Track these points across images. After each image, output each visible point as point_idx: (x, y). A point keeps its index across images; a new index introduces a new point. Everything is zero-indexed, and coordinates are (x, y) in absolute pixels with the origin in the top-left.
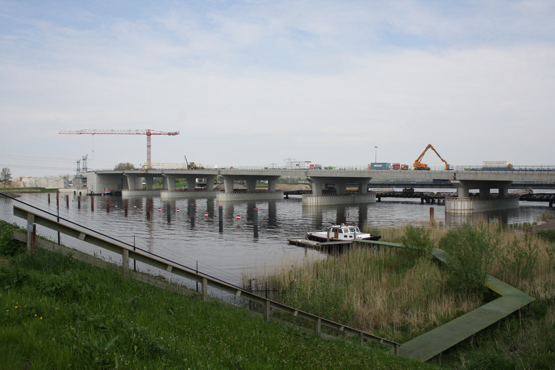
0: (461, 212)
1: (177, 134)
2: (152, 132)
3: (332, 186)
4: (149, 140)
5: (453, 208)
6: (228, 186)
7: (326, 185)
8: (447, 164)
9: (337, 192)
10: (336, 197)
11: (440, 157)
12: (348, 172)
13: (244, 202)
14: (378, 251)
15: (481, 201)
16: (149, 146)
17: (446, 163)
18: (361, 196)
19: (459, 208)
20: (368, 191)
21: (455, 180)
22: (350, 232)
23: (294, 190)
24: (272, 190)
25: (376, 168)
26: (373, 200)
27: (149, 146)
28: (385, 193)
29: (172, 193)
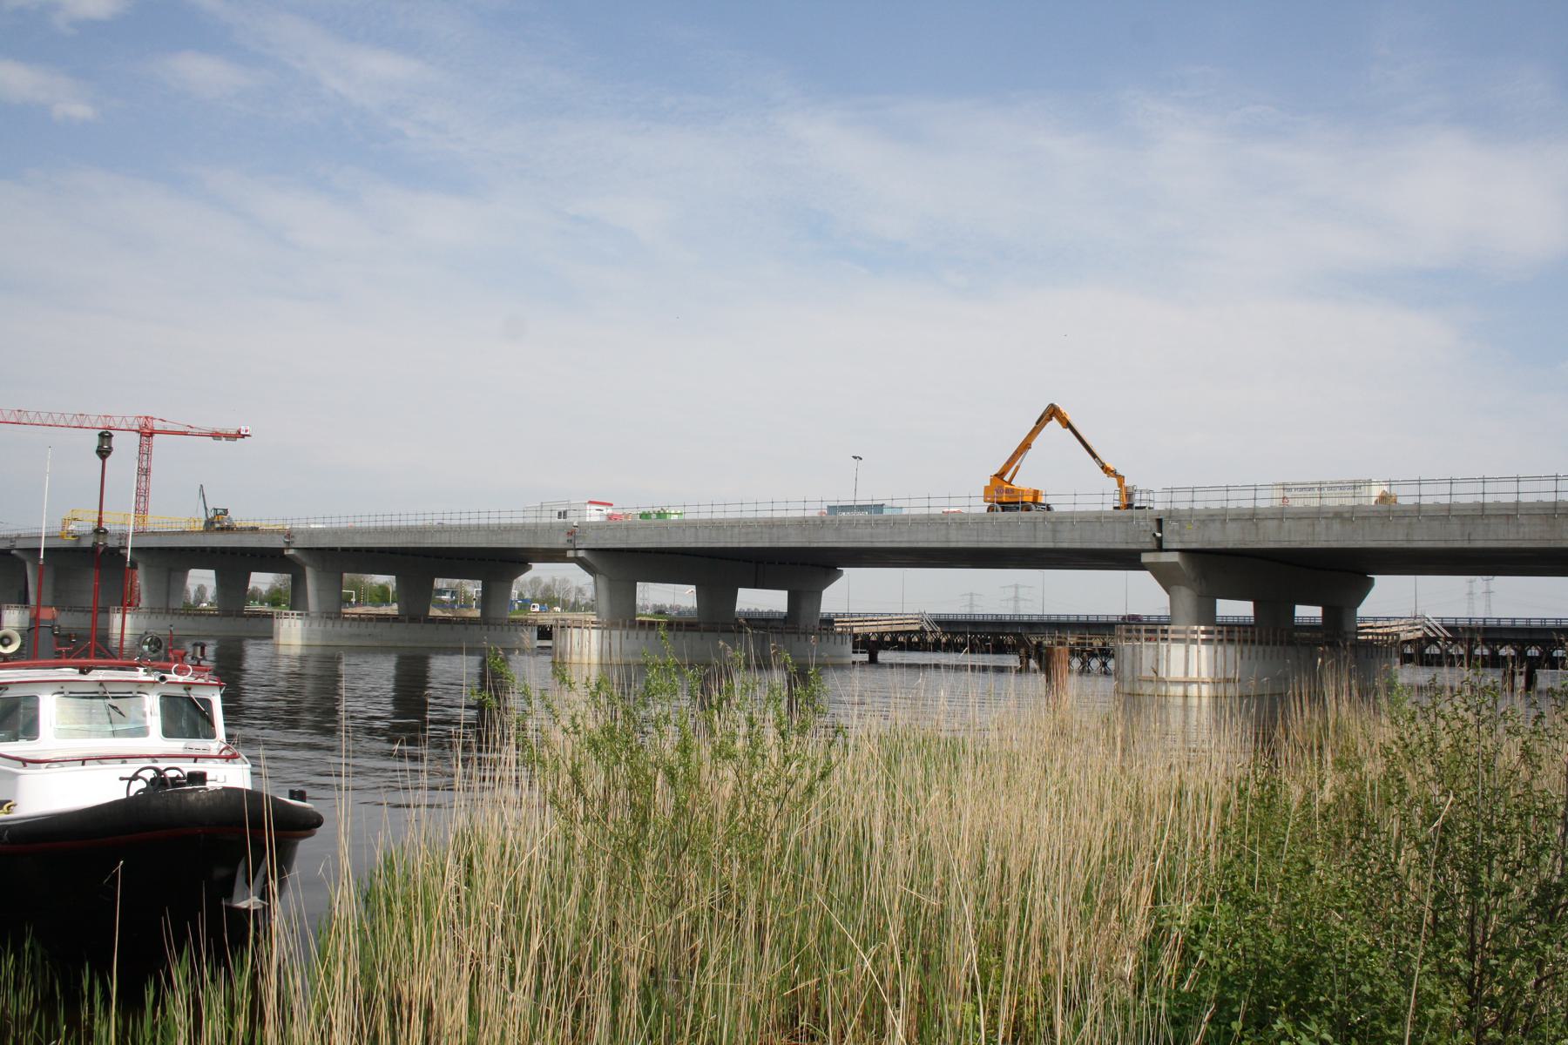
0: (1186, 690)
1: (243, 436)
2: (157, 425)
4: (145, 452)
5: (1147, 672)
8: (1127, 483)
10: (688, 634)
11: (1094, 456)
13: (385, 650)
14: (1512, 695)
15: (1268, 649)
16: (144, 472)
17: (1120, 479)
18: (794, 637)
19: (1177, 672)
21: (1160, 549)
22: (168, 733)
26: (842, 657)
27: (144, 472)
29: (153, 617)
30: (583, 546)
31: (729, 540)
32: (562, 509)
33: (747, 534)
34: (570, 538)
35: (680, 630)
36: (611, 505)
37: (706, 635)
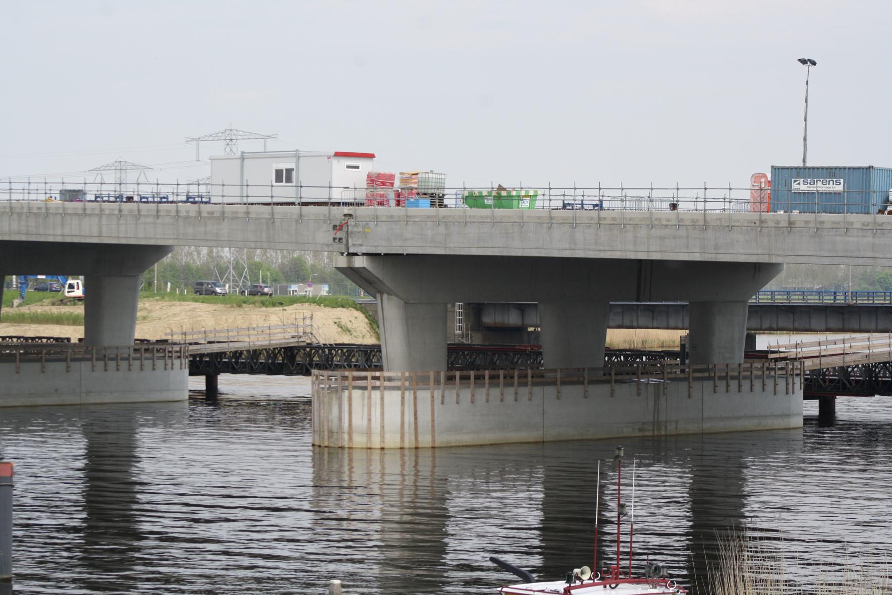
3: (513, 319)
6: (409, 321)
7: (475, 311)
9: (548, 360)
10: (536, 389)
12: (622, 224)
20: (752, 354)
23: (259, 341)
24: (108, 339)
25: (808, 202)
28: (869, 370)
30: (364, 250)
31: (631, 247)
32: (284, 166)
33: (662, 238)
34: (339, 235)
35: (526, 384)
36: (371, 156)
37: (566, 390)
